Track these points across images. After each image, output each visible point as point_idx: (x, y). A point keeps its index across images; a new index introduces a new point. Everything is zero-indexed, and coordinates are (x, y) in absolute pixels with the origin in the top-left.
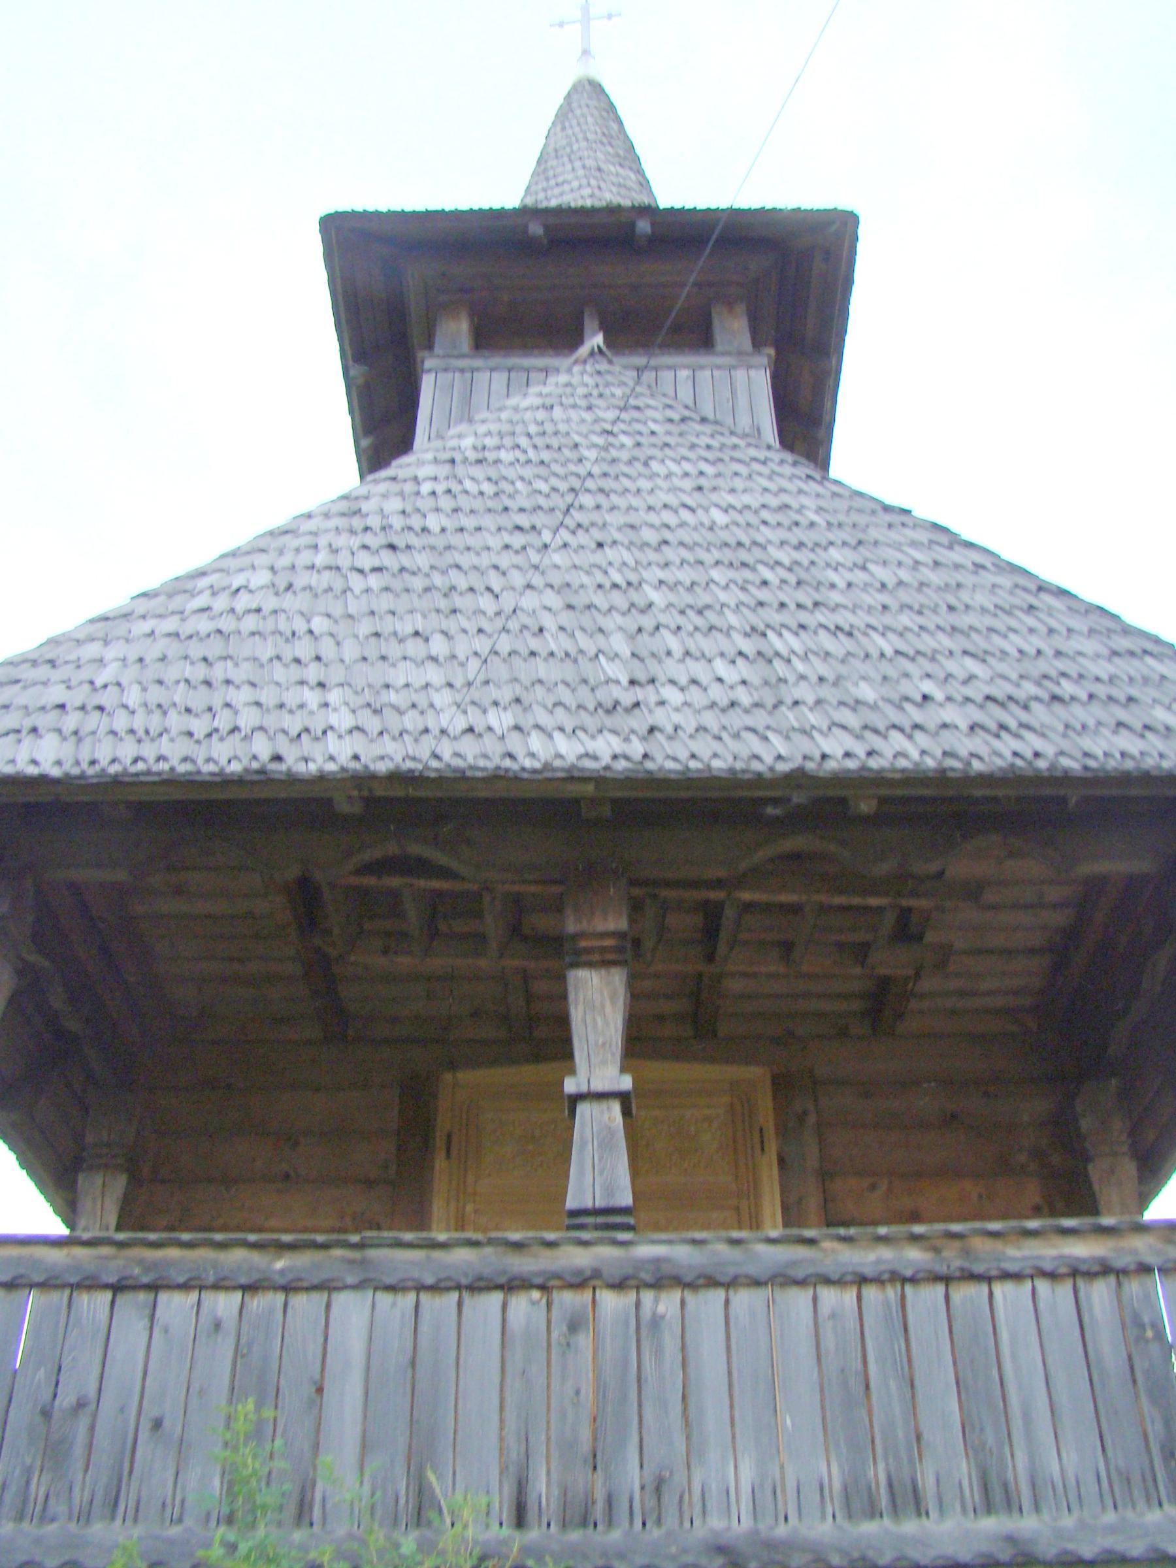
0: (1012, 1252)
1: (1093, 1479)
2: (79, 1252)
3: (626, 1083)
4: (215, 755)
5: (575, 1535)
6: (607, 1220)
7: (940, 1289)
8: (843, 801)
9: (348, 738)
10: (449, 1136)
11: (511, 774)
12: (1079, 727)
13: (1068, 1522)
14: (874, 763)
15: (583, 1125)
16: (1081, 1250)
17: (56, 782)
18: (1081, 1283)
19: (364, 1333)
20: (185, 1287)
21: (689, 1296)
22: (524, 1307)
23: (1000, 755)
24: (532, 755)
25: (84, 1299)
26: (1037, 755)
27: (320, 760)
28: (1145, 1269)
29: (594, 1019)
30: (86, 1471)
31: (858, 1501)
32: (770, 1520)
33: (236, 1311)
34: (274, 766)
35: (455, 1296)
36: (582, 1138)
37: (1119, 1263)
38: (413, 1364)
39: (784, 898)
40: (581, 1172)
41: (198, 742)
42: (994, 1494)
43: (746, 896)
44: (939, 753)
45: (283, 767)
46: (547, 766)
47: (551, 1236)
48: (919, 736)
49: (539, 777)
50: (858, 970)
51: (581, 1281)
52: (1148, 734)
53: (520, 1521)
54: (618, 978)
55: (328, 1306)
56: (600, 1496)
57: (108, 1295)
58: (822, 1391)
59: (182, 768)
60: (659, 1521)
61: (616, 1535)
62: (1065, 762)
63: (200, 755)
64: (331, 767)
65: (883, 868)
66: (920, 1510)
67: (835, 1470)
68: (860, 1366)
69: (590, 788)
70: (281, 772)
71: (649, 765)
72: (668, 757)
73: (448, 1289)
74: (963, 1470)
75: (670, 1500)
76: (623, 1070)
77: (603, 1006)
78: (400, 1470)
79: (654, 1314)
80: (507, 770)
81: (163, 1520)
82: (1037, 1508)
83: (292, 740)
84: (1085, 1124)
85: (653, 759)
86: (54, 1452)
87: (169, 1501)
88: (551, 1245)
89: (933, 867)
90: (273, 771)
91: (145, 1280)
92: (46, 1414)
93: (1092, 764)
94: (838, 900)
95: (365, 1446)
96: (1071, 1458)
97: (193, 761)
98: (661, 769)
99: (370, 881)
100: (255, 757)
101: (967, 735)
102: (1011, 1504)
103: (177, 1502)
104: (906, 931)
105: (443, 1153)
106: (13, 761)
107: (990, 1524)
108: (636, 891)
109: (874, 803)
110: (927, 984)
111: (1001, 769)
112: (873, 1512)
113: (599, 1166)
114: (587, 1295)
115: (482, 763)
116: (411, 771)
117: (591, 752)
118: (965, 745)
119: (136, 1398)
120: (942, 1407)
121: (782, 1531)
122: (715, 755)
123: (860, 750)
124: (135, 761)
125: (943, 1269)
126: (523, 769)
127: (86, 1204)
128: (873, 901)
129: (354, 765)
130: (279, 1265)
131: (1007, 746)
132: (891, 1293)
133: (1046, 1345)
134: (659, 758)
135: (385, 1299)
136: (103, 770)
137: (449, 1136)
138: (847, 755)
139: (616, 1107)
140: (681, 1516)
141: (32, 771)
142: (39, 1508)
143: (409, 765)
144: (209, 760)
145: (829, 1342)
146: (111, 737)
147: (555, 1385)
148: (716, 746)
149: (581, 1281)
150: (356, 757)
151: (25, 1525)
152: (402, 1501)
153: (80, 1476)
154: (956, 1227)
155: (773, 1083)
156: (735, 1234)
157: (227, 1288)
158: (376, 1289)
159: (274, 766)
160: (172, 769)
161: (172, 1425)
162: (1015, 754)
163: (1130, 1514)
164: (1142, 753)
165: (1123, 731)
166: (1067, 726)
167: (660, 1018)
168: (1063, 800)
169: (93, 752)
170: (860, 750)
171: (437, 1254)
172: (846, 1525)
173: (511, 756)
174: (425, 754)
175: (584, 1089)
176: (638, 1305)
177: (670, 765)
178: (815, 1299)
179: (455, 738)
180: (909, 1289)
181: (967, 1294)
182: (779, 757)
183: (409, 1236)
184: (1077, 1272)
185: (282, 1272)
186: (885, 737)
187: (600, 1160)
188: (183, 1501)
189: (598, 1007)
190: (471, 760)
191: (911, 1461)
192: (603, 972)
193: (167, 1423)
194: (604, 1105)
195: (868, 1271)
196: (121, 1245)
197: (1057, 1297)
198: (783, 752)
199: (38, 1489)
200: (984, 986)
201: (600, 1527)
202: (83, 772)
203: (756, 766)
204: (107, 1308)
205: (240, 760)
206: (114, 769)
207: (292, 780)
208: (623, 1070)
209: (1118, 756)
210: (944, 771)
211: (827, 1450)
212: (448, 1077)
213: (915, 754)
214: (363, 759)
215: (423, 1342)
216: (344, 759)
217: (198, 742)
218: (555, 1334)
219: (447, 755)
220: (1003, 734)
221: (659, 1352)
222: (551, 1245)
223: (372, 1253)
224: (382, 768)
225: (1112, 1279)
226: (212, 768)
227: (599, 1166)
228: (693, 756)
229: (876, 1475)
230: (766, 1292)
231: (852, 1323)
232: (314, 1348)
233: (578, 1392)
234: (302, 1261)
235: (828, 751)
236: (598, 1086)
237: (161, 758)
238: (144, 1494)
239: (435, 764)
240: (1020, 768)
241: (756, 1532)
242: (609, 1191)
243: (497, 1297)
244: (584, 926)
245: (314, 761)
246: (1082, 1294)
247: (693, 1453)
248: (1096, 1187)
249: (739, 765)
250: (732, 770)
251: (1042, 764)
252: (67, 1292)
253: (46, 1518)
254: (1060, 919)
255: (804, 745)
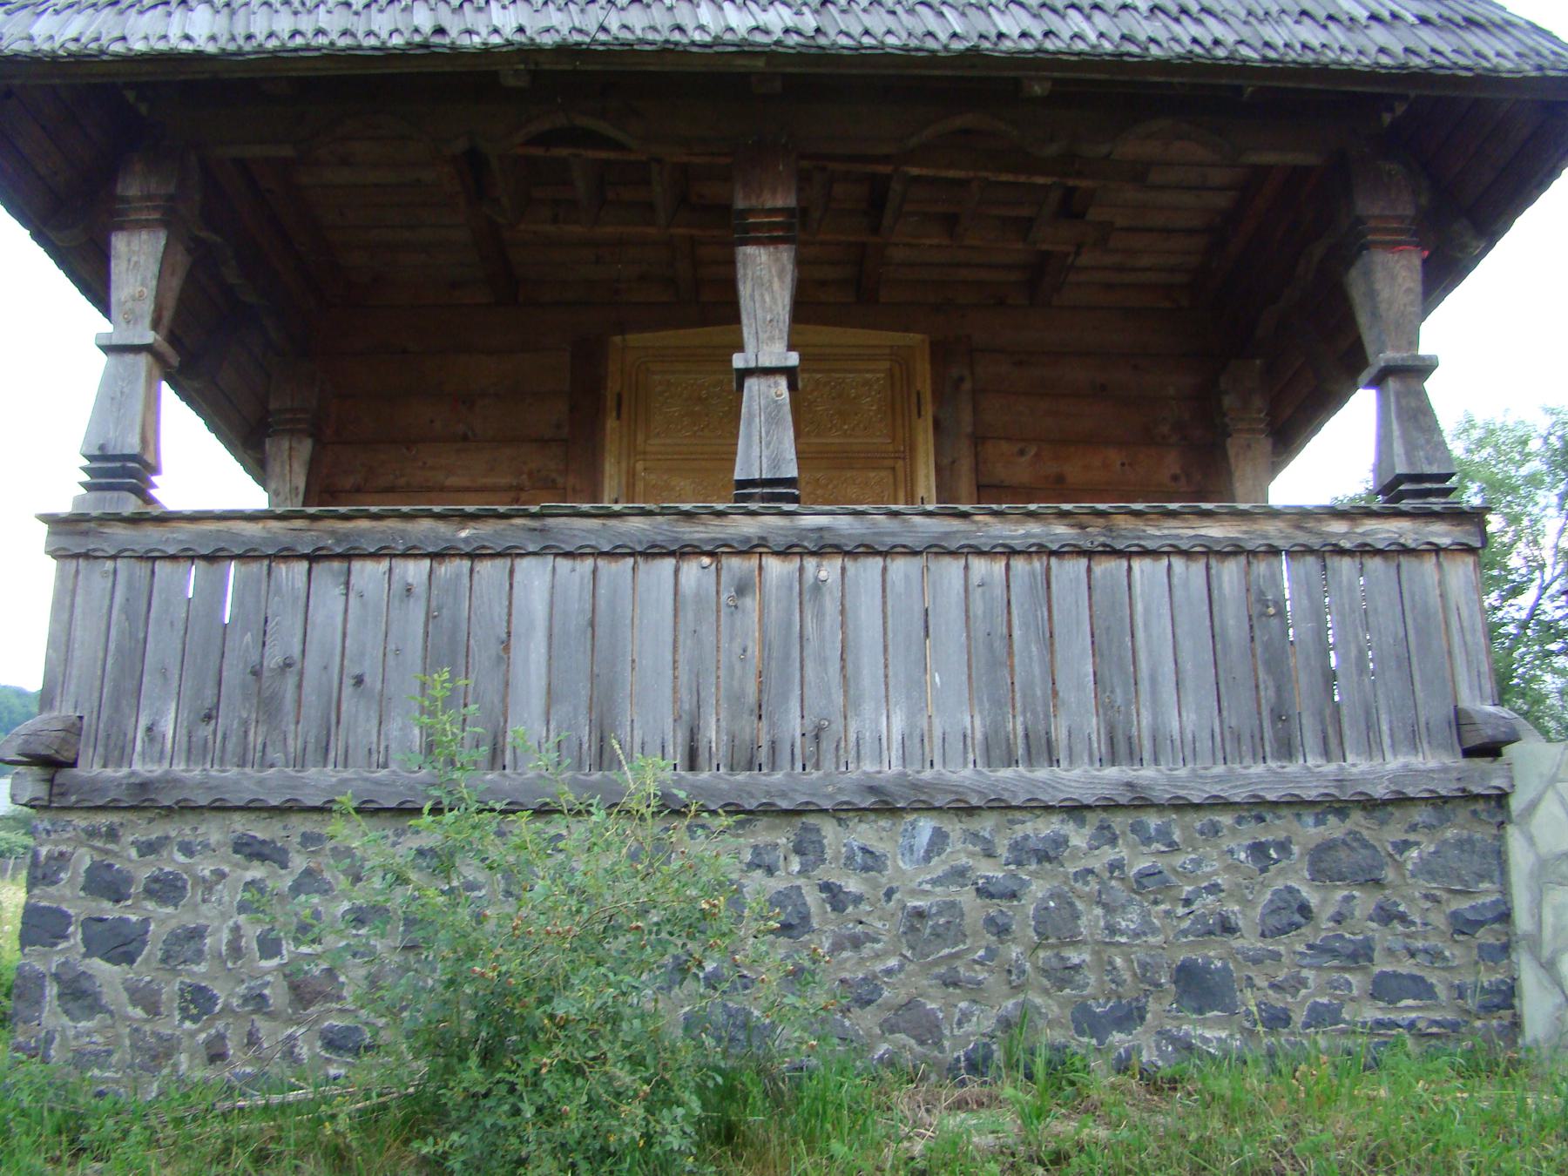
0: (1151, 531)
1: (1208, 736)
2: (275, 525)
3: (793, 359)
4: (375, 28)
5: (742, 777)
6: (776, 492)
7: (1083, 562)
8: (1017, 81)
9: (512, 8)
10: (619, 397)
11: (680, 48)
12: (1261, 13)
13: (1182, 772)
14: (1049, 45)
15: (751, 398)
16: (1215, 531)
17: (211, 58)
18: (1213, 562)
19: (546, 595)
20: (376, 556)
21: (849, 563)
22: (694, 572)
23: (1177, 41)
24: (701, 28)
25: (282, 569)
26: (1217, 42)
27: (484, 32)
28: (1274, 551)
29: (762, 295)
30: (298, 722)
31: (997, 751)
32: (918, 767)
33: (425, 576)
34: (437, 40)
35: (630, 561)
36: (749, 412)
37: (1250, 546)
38: (592, 624)
39: (951, 174)
40: (749, 446)
41: (357, 13)
42: (1119, 747)
43: (915, 171)
44: (1116, 37)
45: (447, 41)
46: (717, 40)
47: (720, 506)
48: (1098, 17)
49: (708, 50)
50: (1020, 246)
51: (751, 548)
52: (1331, 25)
53: (692, 765)
54: (786, 255)
55: (512, 572)
56: (764, 741)
57: (305, 565)
58: (969, 653)
59: (343, 42)
60: (817, 766)
61: (778, 776)
62: (1245, 51)
63: (360, 27)
64: (496, 40)
65: (1052, 150)
66: (1053, 761)
67: (977, 722)
68: (1005, 630)
69: (760, 63)
70: (444, 46)
71: (822, 41)
72: (841, 32)
73: (624, 555)
74: (1093, 724)
75: (827, 745)
76: (791, 347)
77: (771, 282)
78: (583, 720)
79: (816, 578)
80: (677, 44)
81: (370, 765)
82: (1156, 761)
83: (454, 11)
84: (1227, 401)
85: (825, 34)
86: (268, 707)
87: (374, 746)
88: (720, 514)
89: (1104, 149)
90: (436, 46)
91: (339, 550)
92: (256, 673)
93: (1272, 54)
94: (1004, 178)
95: (551, 696)
96: (1190, 718)
97: (353, 35)
98: (834, 44)
99: (538, 152)
100: (417, 30)
101: (1146, 18)
102: (1134, 757)
103: (382, 749)
104: (1071, 208)
105: (614, 414)
106: (165, 37)
107: (1112, 772)
108: (805, 164)
109: (1048, 85)
110: (1084, 260)
111: (1179, 56)
112: (1011, 761)
113: (766, 440)
114: (755, 561)
115: (651, 36)
116: (578, 44)
117: (761, 24)
118: (1145, 29)
119: (337, 659)
120: (1078, 665)
121: (927, 774)
122: (889, 32)
123: (1037, 30)
124: (293, 36)
125: (1087, 545)
126: (693, 43)
127: (275, 467)
128: (1040, 180)
129: (519, 38)
130: (463, 534)
131: (1187, 31)
132: (1038, 564)
133: (1178, 619)
134: (832, 33)
135: (564, 564)
136: (260, 45)
137: (619, 397)
138: (1024, 35)
139: (783, 383)
140: (837, 757)
141: (186, 47)
142: (258, 755)
143: (577, 37)
144: (369, 33)
145: (978, 607)
146: (265, 8)
147: (724, 644)
148: (890, 22)
149: (751, 548)
150: (521, 30)
151: (248, 770)
152: (585, 746)
153: (292, 727)
154: (1101, 506)
155: (933, 354)
156: (894, 507)
157: (415, 556)
158: (556, 555)
159: (437, 40)
160: (332, 44)
161: (373, 681)
162: (1195, 41)
163: (1237, 766)
164: (1324, 46)
165: (1305, 20)
166: (1250, 13)
167: (823, 283)
168: (1239, 90)
169: (248, 26)
170: (1037, 30)
171: (612, 523)
172: (985, 770)
173: (680, 28)
174: (592, 27)
175: (752, 365)
176: (801, 569)
177: (844, 41)
178: (966, 567)
179: (623, 9)
180: (1053, 561)
181: (1106, 568)
182: (955, 35)
183: (585, 507)
184: (1212, 552)
185: (466, 540)
186: (1063, 17)
187: (767, 433)
188: (387, 747)
189: (766, 283)
190: (639, 33)
191: (1047, 716)
192: (772, 249)
193: (367, 679)
194: (771, 380)
195: (1017, 544)
196: (314, 518)
197: (1190, 573)
198: (958, 30)
199: (256, 737)
200: (1146, 261)
201: (765, 770)
202: (240, 47)
203: (931, 44)
204: (305, 579)
205: (402, 33)
206: (272, 44)
207: (456, 53)
208: (791, 348)
209: (1298, 47)
210: (1122, 55)
211: (971, 706)
212: (617, 339)
213: (1092, 37)
214: (528, 32)
215: (602, 604)
216: (509, 31)
217: (357, 13)
218: (724, 597)
219: (614, 26)
220: (1184, 18)
221: (820, 615)
222: (720, 514)
223: (550, 521)
224: (548, 40)
225: (1242, 559)
226: (373, 41)
227: (766, 440)
228: (867, 32)
229: (1014, 728)
230: (917, 562)
231: (999, 591)
232: (500, 610)
233: (745, 651)
234: (486, 529)
235: (1004, 30)
236: (766, 361)
237: (320, 32)
238: (351, 741)
239: (602, 37)
240: (1199, 56)
241: (905, 775)
242: (776, 463)
243: (669, 563)
244: (754, 202)
245: (478, 34)
246: (1213, 571)
247: (851, 703)
248: (1232, 460)
249: (913, 43)
250: (905, 48)
251: (1220, 53)
252: (266, 562)
253: (266, 764)
254: (1222, 201)
255: (979, 23)
